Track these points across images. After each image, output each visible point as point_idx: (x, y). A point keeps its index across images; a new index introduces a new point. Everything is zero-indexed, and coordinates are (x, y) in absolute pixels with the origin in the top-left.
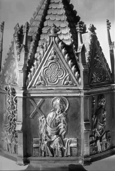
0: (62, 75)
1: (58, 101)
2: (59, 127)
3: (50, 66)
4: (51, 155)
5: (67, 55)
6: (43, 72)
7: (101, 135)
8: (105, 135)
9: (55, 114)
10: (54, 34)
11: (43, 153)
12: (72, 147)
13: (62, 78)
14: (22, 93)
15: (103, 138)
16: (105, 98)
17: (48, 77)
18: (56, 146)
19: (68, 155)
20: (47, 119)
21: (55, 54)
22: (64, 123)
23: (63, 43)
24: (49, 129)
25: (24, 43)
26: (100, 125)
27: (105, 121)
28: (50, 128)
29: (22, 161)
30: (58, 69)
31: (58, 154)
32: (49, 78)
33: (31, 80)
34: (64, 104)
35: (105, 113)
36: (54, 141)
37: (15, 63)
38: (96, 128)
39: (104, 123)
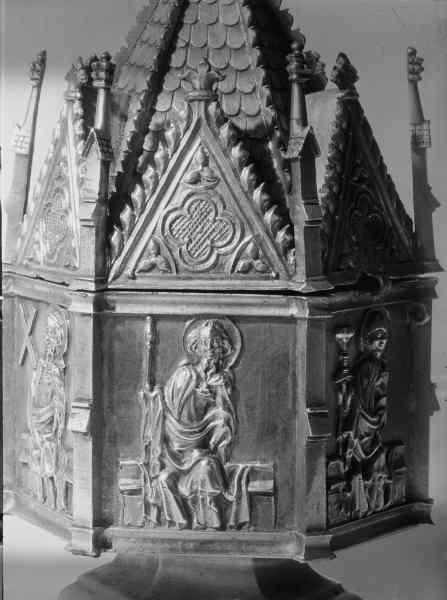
0: (228, 239)
1: (205, 331)
3: (187, 204)
4: (179, 519)
7: (366, 454)
8: (383, 456)
9: (194, 378)
10: (206, 94)
11: (154, 512)
13: (229, 248)
14: (92, 300)
15: (376, 464)
17: (180, 245)
18: (200, 489)
19: (242, 521)
20: (168, 391)
21: (205, 163)
23: (233, 127)
24: (173, 426)
25: (99, 123)
27: (383, 408)
28: (180, 427)
31: (205, 517)
32: (184, 247)
33: (119, 255)
34: (226, 342)
37: (67, 195)
38: (351, 430)
39: (380, 412)
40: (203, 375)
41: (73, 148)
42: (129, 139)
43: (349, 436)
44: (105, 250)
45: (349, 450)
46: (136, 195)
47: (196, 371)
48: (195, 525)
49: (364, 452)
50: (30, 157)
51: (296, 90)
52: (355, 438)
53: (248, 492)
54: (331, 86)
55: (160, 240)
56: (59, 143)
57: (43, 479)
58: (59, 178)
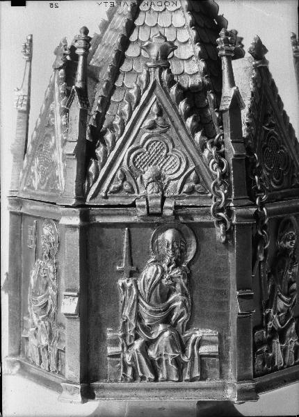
0: (177, 168)
2: (170, 304)
4: (150, 375)
7: (282, 325)
9: (160, 271)
15: (288, 332)
22: (184, 294)
23: (180, 87)
24: (145, 309)
25: (79, 85)
27: (294, 291)
40: (166, 269)
41: (58, 104)
42: (99, 101)
43: (270, 313)
44: (83, 175)
45: (270, 323)
46: (99, 151)
47: (161, 266)
48: (160, 379)
49: (280, 323)
50: (27, 112)
51: (224, 60)
52: (274, 314)
53: (198, 354)
54: (248, 55)
55: (126, 169)
56: (50, 100)
57: (39, 349)
58: (49, 126)
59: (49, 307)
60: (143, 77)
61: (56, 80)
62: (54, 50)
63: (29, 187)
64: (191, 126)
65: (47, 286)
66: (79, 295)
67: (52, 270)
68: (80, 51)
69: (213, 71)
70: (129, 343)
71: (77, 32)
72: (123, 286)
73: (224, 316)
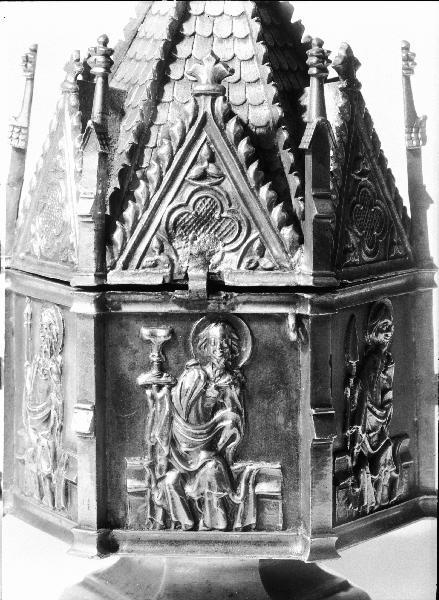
2: (216, 424)
4: (186, 521)
5: (254, 167)
6: (167, 223)
7: (373, 448)
8: (390, 449)
9: (202, 378)
11: (160, 513)
12: (263, 496)
15: (382, 460)
16: (390, 319)
18: (207, 490)
21: (212, 159)
22: (236, 410)
23: (240, 122)
24: (180, 428)
26: (374, 413)
27: (389, 401)
29: (85, 539)
30: (222, 212)
33: (123, 249)
35: (391, 372)
36: (197, 471)
43: (356, 432)
45: (357, 445)
56: (55, 135)
59: (52, 422)
60: (189, 108)
61: (66, 109)
62: (63, 66)
63: (28, 253)
64: (235, 131)
65: (48, 392)
66: (95, 409)
67: (55, 369)
68: (98, 70)
69: (289, 100)
70: (158, 476)
71: (94, 42)
72: (153, 397)
73: (292, 441)
